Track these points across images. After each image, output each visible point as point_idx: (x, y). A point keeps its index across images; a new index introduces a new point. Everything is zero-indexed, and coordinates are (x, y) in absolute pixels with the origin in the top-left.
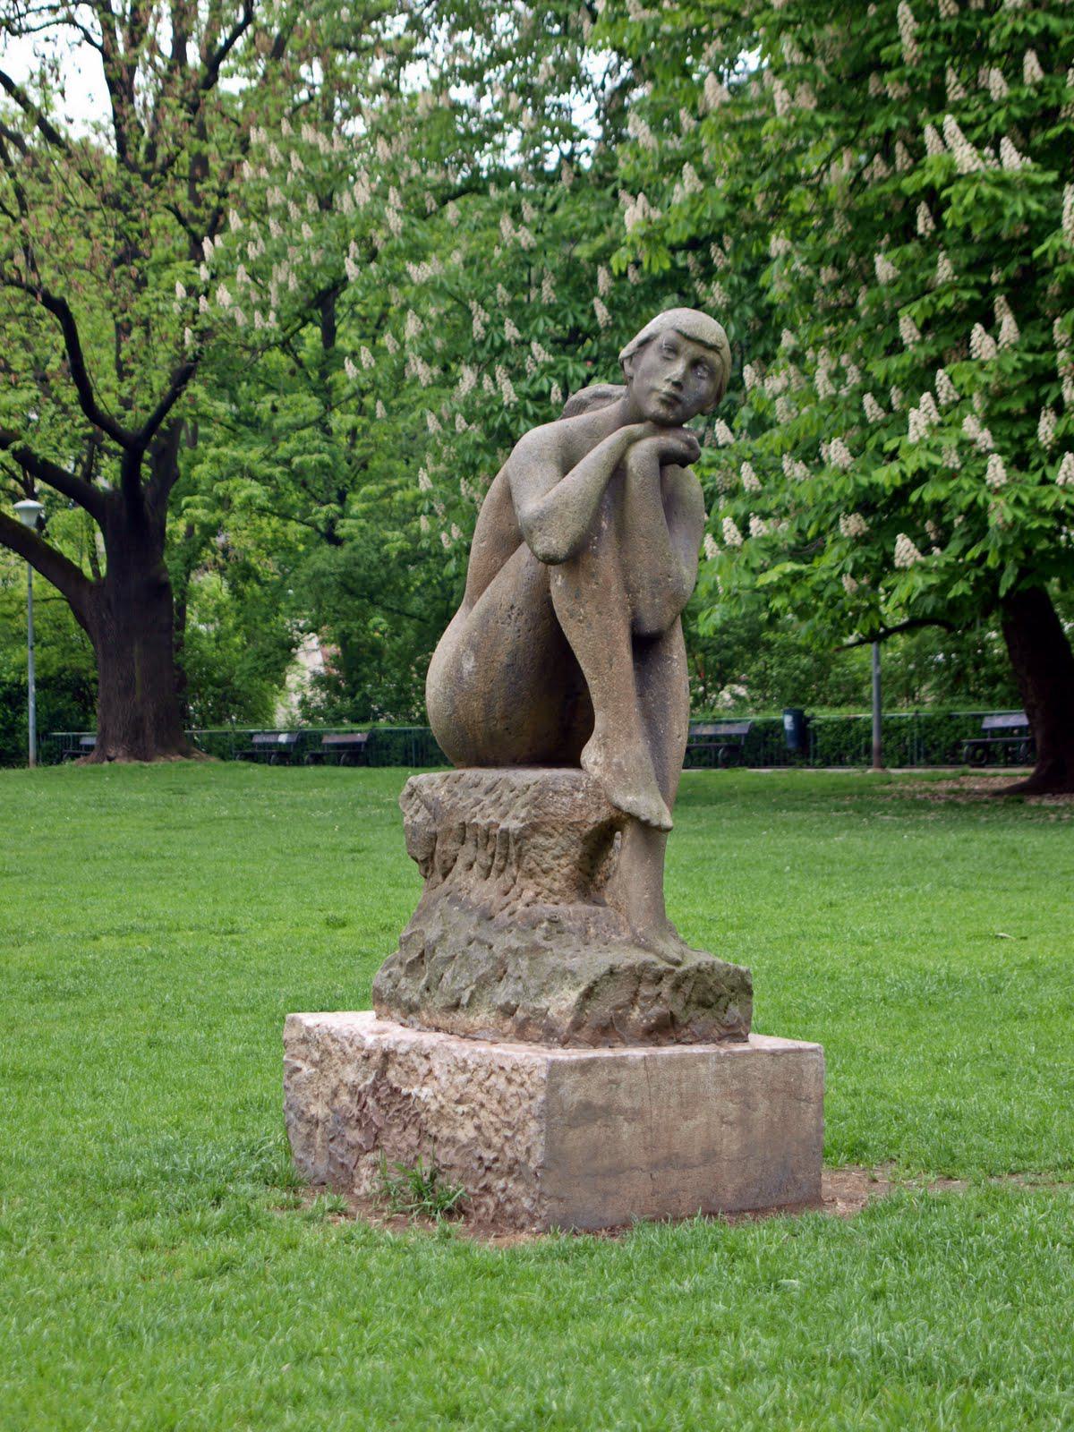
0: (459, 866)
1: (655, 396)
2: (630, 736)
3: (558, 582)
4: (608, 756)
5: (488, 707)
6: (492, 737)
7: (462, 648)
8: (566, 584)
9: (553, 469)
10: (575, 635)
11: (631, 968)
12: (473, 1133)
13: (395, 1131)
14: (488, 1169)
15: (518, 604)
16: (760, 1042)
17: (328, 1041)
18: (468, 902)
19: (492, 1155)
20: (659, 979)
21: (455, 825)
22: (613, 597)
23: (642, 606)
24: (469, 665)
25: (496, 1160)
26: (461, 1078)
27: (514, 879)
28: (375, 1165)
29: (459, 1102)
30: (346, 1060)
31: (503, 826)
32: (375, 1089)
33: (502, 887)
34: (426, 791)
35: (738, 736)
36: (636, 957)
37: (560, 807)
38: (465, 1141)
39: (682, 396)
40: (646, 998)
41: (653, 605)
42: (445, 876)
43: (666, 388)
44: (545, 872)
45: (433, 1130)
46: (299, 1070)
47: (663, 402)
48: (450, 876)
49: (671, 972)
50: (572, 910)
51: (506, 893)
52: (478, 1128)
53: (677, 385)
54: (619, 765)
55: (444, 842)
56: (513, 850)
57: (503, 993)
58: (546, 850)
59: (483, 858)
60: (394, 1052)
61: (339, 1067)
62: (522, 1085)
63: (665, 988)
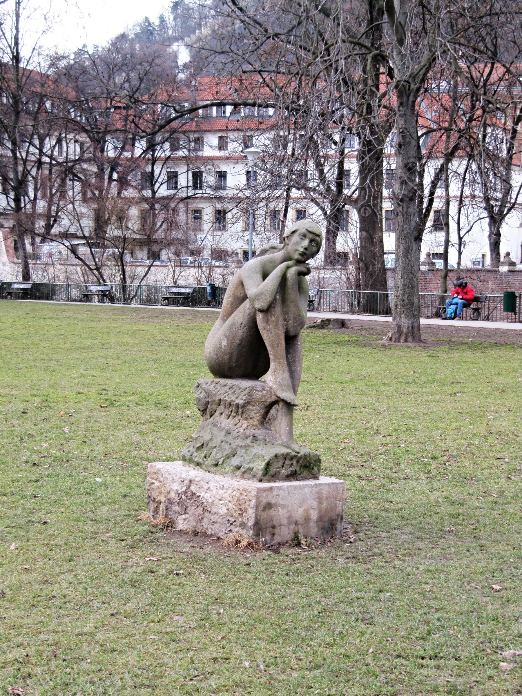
0: (217, 413)
1: (297, 252)
2: (283, 372)
3: (260, 317)
4: (275, 378)
5: (230, 358)
6: (230, 368)
7: (222, 337)
8: (263, 318)
9: (259, 277)
10: (265, 335)
11: (283, 454)
12: (226, 511)
13: (193, 508)
14: (231, 524)
15: (244, 323)
16: (323, 480)
17: (167, 474)
18: (220, 426)
19: (233, 520)
20: (292, 458)
21: (217, 399)
22: (280, 323)
23: (290, 327)
24: (224, 343)
25: (235, 521)
26: (221, 492)
27: (240, 420)
28: (185, 520)
29: (220, 500)
30: (174, 481)
31: (237, 402)
32: (185, 493)
33: (235, 423)
34: (204, 386)
35: (189, 293)
36: (285, 450)
37: (257, 395)
38: (222, 514)
39: (307, 252)
40: (287, 465)
41: (294, 326)
42: (211, 416)
43: (302, 250)
44: (251, 418)
45: (209, 509)
46: (153, 483)
47: (300, 254)
48: (213, 417)
49: (297, 456)
50: (260, 432)
51: (236, 425)
52: (228, 509)
53: (306, 249)
54: (279, 382)
55: (212, 405)
56: (240, 410)
57: (235, 461)
58: (252, 410)
59: (227, 412)
60: (194, 480)
61: (171, 483)
62: (246, 496)
63: (294, 462)
